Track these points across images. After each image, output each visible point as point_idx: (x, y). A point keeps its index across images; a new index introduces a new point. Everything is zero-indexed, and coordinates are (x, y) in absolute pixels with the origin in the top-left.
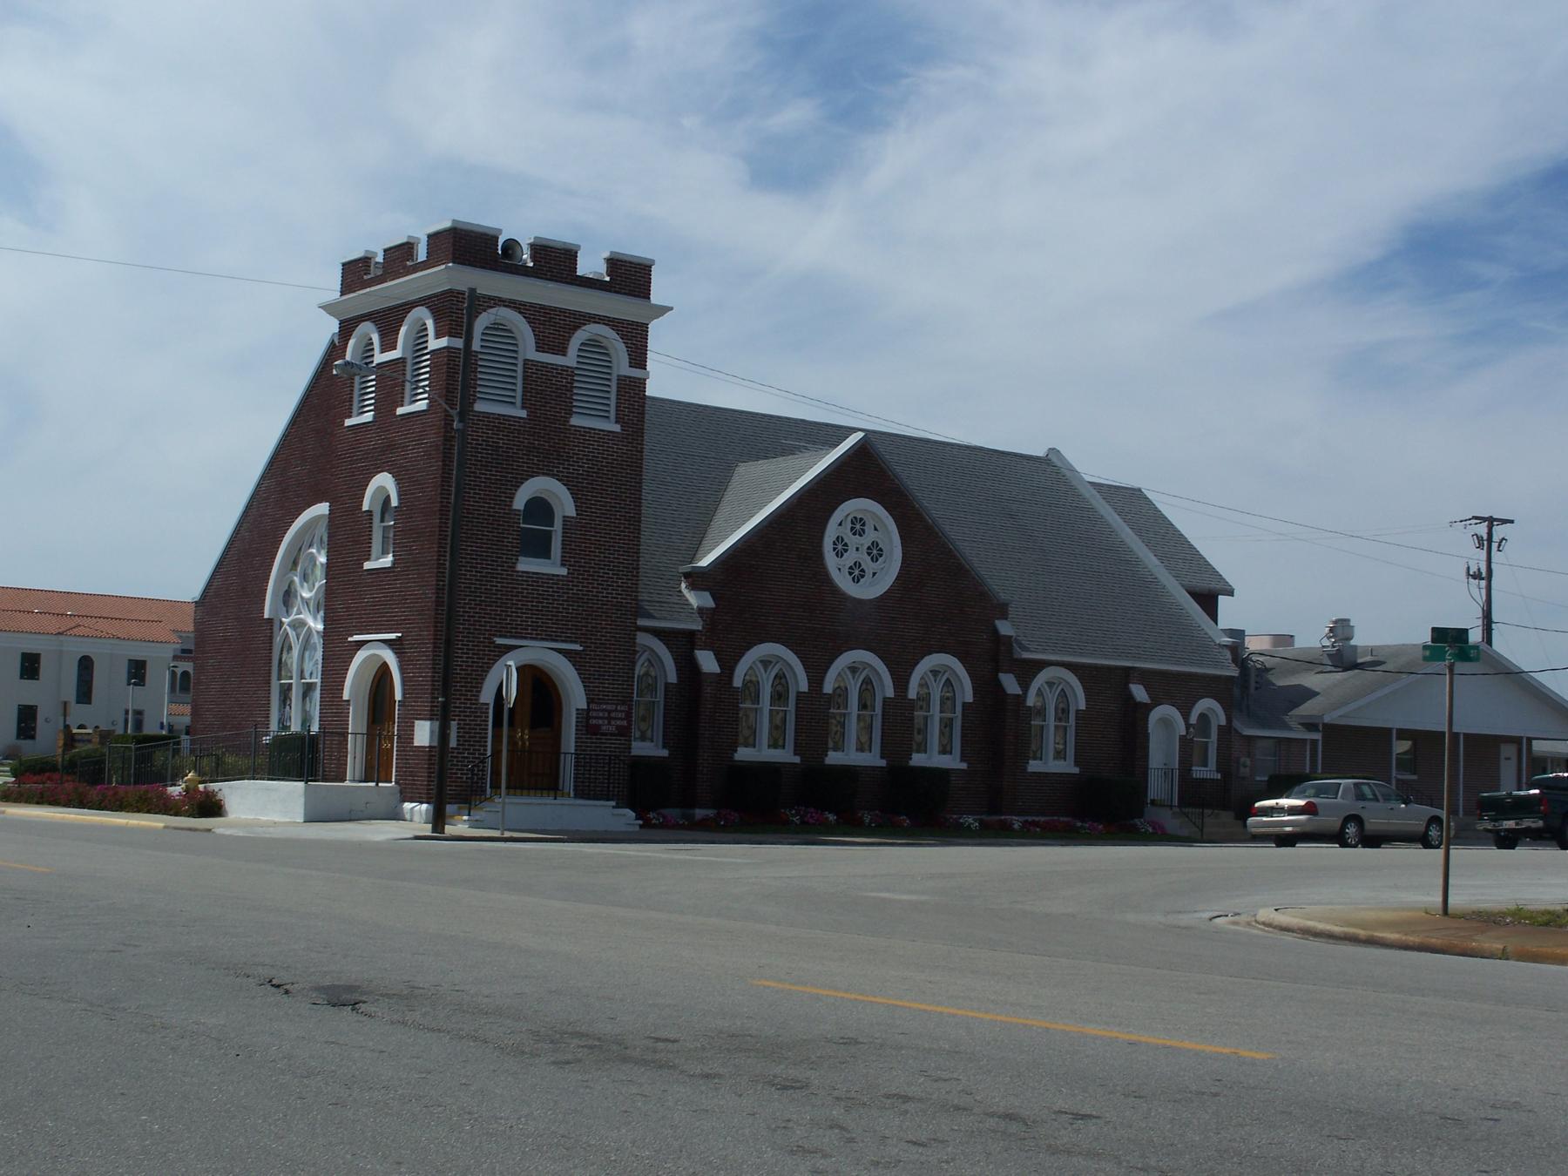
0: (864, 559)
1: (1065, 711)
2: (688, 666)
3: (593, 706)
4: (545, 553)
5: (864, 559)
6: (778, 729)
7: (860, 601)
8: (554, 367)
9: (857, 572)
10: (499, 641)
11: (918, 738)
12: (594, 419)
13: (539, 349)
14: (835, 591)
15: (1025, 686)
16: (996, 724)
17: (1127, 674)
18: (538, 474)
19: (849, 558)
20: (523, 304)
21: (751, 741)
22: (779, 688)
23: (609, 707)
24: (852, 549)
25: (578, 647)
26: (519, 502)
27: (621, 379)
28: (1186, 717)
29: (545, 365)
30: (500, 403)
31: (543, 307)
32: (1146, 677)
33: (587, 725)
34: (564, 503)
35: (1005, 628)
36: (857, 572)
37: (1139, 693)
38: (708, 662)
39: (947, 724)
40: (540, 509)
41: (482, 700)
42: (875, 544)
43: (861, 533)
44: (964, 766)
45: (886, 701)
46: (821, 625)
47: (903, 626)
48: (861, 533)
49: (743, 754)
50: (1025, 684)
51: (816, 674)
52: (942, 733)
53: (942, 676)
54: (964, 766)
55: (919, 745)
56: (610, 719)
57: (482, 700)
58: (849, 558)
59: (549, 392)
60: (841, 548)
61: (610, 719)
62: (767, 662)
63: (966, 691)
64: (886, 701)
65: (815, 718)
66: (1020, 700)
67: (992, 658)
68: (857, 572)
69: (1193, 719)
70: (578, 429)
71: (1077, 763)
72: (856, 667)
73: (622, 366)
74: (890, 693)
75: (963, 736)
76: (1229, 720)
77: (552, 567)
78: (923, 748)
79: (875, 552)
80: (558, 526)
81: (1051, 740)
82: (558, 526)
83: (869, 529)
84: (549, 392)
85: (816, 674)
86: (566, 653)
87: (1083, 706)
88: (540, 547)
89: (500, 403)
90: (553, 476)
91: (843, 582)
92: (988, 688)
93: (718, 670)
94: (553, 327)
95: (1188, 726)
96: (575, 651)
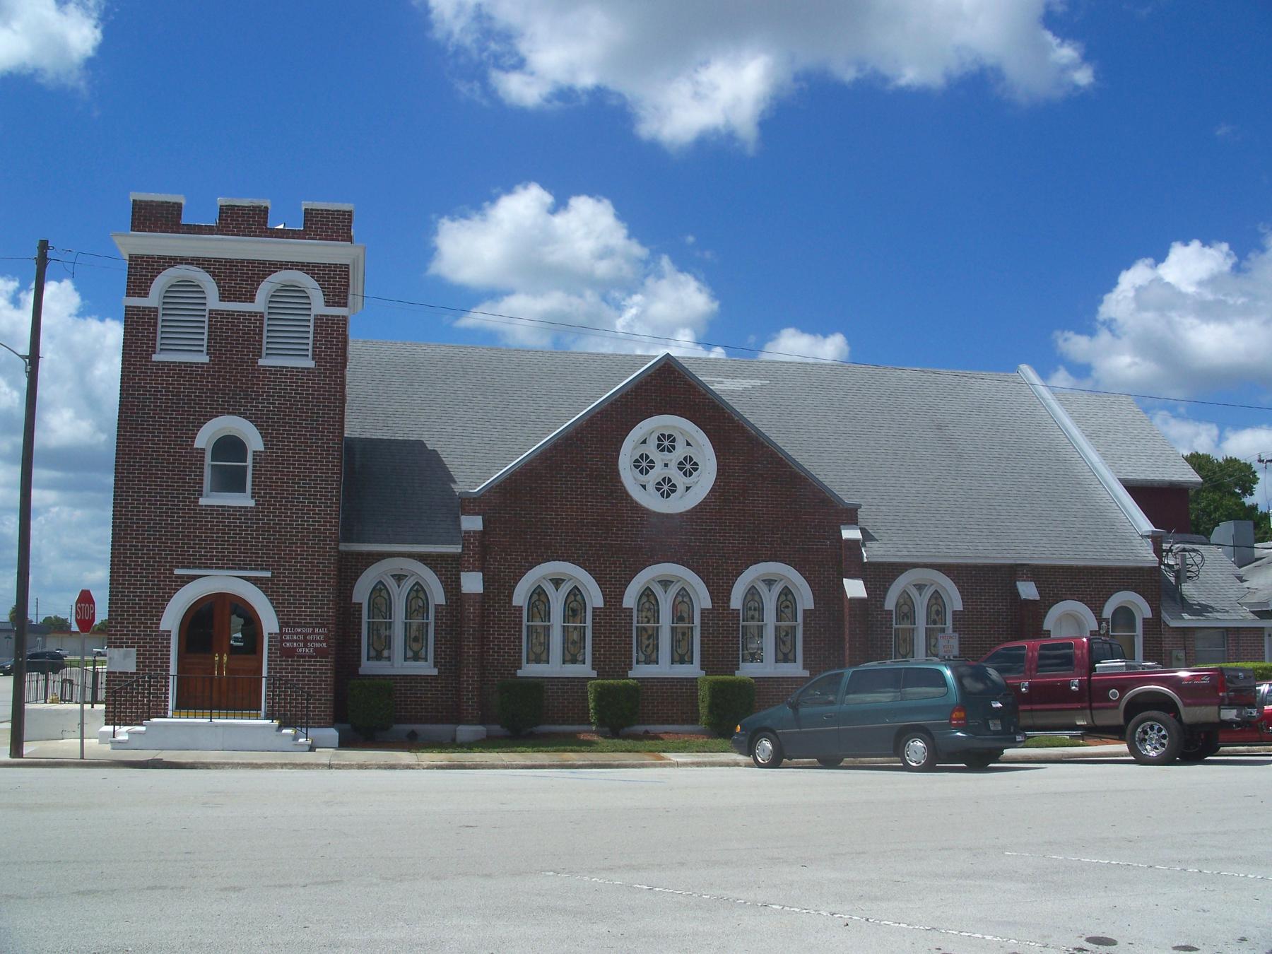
0: (669, 473)
1: (941, 613)
2: (452, 586)
3: (285, 630)
4: (242, 489)
5: (669, 473)
6: (414, 641)
8: (241, 314)
9: (666, 488)
10: (177, 572)
12: (289, 357)
13: (327, 304)
17: (1014, 572)
18: (223, 414)
20: (208, 260)
21: (544, 657)
22: (574, 605)
23: (305, 630)
24: (673, 465)
25: (268, 574)
26: (205, 437)
27: (319, 319)
28: (1098, 612)
29: (231, 313)
30: (185, 352)
31: (227, 260)
32: (1036, 573)
33: (283, 651)
34: (254, 441)
36: (666, 488)
37: (1028, 590)
38: (472, 583)
40: (230, 447)
41: (163, 627)
46: (619, 540)
47: (714, 540)
48: (671, 449)
49: (530, 670)
53: (769, 580)
56: (306, 641)
57: (163, 626)
59: (235, 339)
60: (643, 464)
61: (306, 641)
62: (556, 579)
65: (615, 635)
67: (827, 560)
68: (666, 487)
69: (1108, 612)
70: (267, 369)
71: (806, 666)
72: (669, 582)
73: (319, 307)
76: (1156, 611)
77: (244, 500)
78: (754, 657)
80: (249, 462)
82: (249, 462)
84: (235, 339)
86: (255, 581)
88: (232, 481)
89: (185, 352)
90: (240, 415)
91: (650, 501)
92: (829, 592)
93: (865, 595)
94: (238, 278)
95: (1100, 620)
96: (267, 579)
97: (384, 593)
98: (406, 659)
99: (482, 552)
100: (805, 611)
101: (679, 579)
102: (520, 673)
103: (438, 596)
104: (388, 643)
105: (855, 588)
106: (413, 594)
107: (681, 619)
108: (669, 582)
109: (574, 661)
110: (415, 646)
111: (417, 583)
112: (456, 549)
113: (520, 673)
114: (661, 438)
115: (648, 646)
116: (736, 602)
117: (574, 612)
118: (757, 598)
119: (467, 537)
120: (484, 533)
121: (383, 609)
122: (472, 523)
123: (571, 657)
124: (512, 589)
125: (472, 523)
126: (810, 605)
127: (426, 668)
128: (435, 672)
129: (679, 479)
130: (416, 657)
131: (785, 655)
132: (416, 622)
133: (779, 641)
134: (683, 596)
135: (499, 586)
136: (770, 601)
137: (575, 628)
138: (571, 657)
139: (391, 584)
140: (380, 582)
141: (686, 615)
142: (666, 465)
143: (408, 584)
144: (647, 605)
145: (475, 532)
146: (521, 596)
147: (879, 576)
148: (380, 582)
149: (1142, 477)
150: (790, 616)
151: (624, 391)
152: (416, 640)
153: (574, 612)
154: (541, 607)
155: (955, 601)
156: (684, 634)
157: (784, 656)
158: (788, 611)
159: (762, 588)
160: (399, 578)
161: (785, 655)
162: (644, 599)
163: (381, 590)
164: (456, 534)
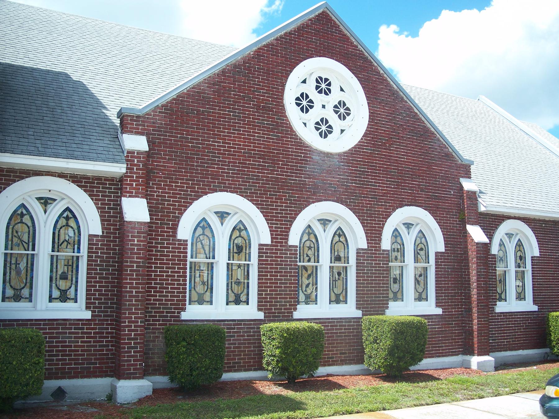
2: (112, 215)
6: (63, 275)
7: (328, 155)
11: (395, 287)
14: (300, 144)
15: (490, 236)
16: (464, 275)
19: (315, 115)
21: (207, 297)
22: (239, 241)
35: (467, 185)
36: (324, 129)
38: (136, 210)
39: (421, 278)
42: (342, 104)
43: (327, 92)
44: (439, 311)
45: (359, 252)
46: (281, 177)
48: (327, 92)
49: (193, 312)
50: (490, 231)
51: (280, 226)
52: (417, 281)
53: (413, 225)
54: (439, 311)
55: (395, 294)
58: (315, 115)
60: (305, 104)
63: (437, 243)
64: (359, 252)
66: (486, 247)
67: (456, 208)
71: (535, 302)
72: (326, 220)
74: (363, 244)
75: (437, 282)
78: (310, 299)
79: (342, 110)
81: (512, 284)
83: (335, 88)
85: (280, 226)
87: (537, 253)
91: (309, 136)
92: (456, 238)
93: (147, 219)
97: (26, 219)
98: (51, 299)
99: (146, 175)
100: (437, 254)
101: (338, 218)
102: (184, 316)
103: (92, 223)
104: (30, 283)
105: (476, 233)
106: (63, 222)
107: (338, 259)
108: (326, 220)
109: (237, 301)
110: (63, 284)
111: (68, 209)
112: (118, 169)
113: (184, 316)
114: (319, 80)
115: (307, 286)
116: (294, 239)
117: (240, 249)
118: (399, 240)
119: (131, 157)
120: (148, 155)
121: (25, 238)
122: (136, 143)
123: (237, 298)
124: (176, 221)
125: (136, 143)
126: (442, 249)
127: (77, 310)
128: (88, 315)
129: (333, 119)
130: (64, 297)
131: (338, 296)
132: (66, 253)
133: (231, 282)
134: (339, 236)
135: (165, 216)
136: (325, 240)
137: (239, 266)
138: (421, 297)
139: (36, 208)
140: (23, 206)
141: (342, 255)
142: (324, 107)
143: (56, 210)
144: (308, 244)
145: (139, 153)
146: (185, 230)
147: (490, 223)
148: (23, 206)
149: (436, 122)
150: (424, 257)
151: (288, 30)
152: (64, 277)
153: (240, 249)
154: (206, 242)
155: (533, 248)
156: (339, 274)
157: (338, 298)
158: (422, 253)
159: (214, 221)
160: (46, 202)
161: (338, 296)
162: (200, 231)
163: (22, 215)
164: (117, 152)
